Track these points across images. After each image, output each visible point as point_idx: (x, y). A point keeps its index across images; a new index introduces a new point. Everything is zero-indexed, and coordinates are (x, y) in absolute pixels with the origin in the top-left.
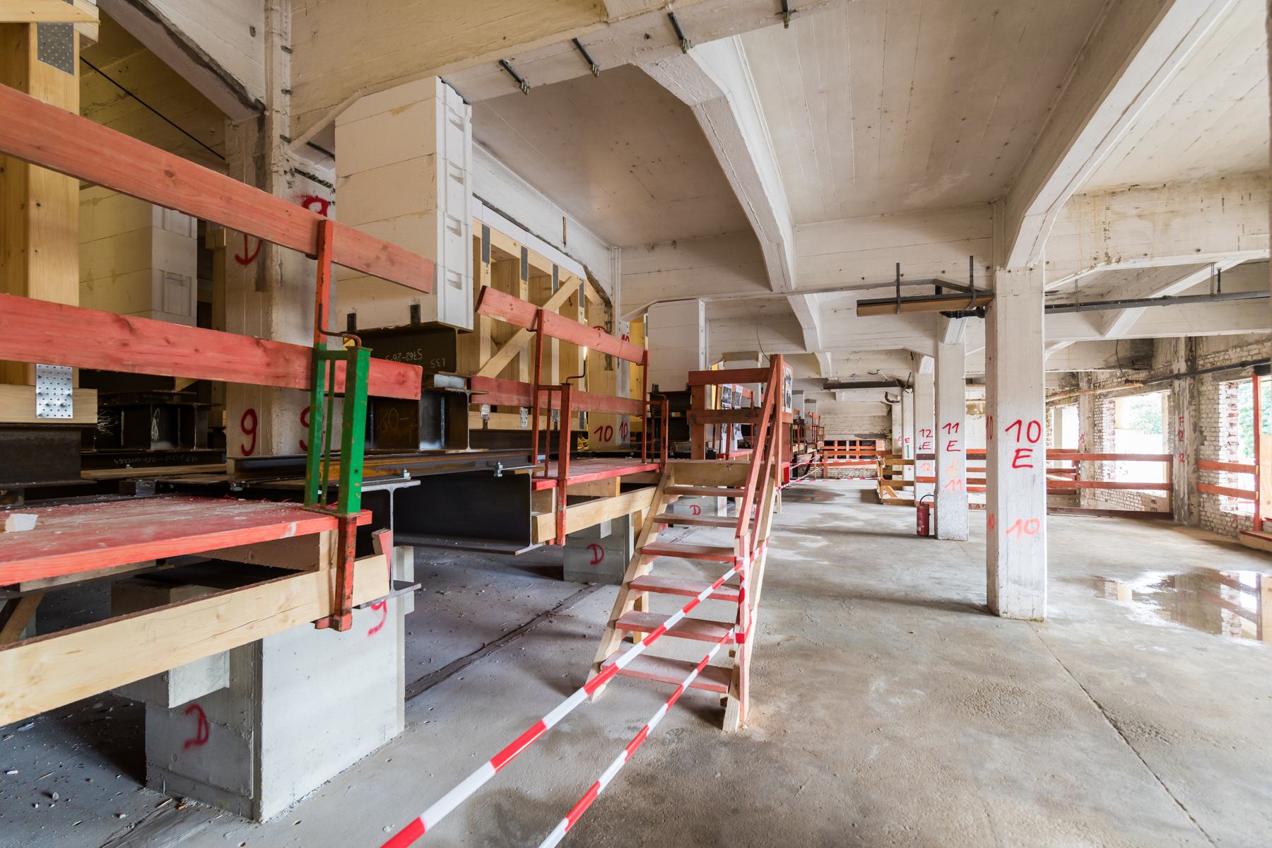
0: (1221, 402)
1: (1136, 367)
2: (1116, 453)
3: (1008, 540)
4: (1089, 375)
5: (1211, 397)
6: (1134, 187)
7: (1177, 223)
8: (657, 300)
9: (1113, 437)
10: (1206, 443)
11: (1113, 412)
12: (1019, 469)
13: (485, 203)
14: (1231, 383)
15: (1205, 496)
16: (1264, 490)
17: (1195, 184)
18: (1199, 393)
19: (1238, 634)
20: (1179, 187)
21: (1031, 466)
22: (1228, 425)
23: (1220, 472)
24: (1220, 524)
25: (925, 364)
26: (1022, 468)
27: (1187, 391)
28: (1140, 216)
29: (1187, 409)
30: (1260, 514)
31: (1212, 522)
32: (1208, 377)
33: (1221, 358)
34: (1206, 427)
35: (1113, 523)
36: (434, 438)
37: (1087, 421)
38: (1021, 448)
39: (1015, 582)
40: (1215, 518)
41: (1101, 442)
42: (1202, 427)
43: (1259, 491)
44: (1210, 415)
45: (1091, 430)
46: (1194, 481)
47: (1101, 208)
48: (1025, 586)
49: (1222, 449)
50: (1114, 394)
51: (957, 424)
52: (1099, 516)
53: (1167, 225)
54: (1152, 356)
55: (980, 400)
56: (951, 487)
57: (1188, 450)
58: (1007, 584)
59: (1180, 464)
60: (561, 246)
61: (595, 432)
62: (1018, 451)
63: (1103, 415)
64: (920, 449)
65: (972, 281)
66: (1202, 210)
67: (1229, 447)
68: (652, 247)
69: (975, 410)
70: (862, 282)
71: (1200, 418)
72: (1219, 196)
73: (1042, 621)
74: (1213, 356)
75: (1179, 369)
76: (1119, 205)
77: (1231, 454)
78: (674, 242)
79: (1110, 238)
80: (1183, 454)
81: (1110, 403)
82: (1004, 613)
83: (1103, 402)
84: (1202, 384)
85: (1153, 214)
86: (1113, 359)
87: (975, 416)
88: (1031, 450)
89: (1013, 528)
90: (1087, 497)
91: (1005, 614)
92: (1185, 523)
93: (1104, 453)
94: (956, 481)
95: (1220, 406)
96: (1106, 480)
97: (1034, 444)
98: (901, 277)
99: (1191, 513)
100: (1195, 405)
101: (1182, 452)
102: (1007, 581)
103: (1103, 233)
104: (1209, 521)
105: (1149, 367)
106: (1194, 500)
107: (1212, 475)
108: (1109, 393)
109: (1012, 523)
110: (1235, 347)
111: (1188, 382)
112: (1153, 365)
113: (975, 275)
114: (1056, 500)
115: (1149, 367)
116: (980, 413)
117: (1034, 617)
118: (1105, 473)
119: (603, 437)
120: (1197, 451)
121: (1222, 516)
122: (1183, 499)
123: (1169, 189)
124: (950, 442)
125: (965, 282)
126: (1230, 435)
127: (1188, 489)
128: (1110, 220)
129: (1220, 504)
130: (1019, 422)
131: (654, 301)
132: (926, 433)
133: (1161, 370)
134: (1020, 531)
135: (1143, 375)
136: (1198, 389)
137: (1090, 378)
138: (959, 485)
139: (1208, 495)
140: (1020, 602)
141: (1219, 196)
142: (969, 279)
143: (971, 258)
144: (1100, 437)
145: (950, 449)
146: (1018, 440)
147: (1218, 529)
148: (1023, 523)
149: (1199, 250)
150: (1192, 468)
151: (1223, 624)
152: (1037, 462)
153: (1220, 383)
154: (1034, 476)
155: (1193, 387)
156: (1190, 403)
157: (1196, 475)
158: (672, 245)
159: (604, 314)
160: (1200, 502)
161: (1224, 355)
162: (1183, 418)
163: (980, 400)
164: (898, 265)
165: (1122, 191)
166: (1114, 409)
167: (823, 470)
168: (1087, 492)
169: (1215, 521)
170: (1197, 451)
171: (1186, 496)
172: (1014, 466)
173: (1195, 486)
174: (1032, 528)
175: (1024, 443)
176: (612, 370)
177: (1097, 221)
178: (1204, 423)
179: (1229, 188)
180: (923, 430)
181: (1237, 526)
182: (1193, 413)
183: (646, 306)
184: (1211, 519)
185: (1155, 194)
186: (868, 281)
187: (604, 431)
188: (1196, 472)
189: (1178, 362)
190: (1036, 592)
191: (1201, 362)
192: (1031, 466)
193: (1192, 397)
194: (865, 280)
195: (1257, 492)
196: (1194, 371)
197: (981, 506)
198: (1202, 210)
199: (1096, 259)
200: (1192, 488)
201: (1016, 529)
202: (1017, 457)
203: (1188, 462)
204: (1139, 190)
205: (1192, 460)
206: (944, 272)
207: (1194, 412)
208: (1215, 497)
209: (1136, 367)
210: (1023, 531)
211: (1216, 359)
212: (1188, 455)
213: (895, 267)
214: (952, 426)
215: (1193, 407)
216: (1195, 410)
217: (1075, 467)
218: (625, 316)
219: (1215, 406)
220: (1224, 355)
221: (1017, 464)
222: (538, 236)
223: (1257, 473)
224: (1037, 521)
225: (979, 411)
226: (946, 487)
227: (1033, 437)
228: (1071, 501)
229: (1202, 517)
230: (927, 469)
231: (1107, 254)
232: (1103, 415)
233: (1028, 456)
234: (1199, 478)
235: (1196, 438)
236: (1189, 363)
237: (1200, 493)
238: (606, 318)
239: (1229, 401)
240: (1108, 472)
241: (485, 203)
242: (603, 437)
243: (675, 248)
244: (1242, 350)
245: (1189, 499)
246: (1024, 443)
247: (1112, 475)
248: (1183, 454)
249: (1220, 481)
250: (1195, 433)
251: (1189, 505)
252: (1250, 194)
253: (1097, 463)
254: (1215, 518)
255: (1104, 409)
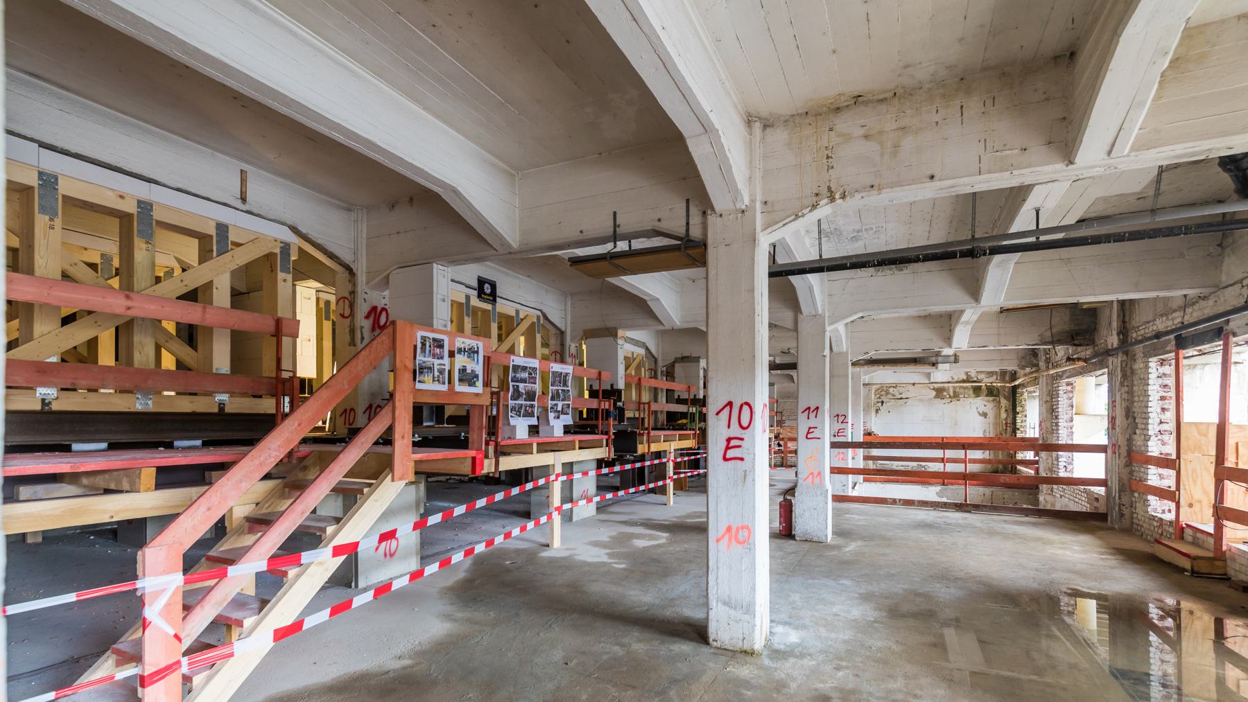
0: (1150, 382)
1: (1076, 342)
2: (1075, 443)
3: (718, 551)
4: (1047, 354)
5: (1142, 377)
6: (857, 99)
7: (908, 142)
8: (396, 266)
9: (1071, 424)
10: (1138, 431)
11: (1071, 395)
12: (729, 462)
13: (43, 145)
14: (1163, 360)
15: (1136, 495)
16: (1185, 489)
17: (930, 89)
18: (1133, 372)
19: (1169, 662)
20: (911, 95)
21: (742, 459)
22: (1159, 410)
23: (1149, 466)
24: (1148, 529)
25: (836, 341)
26: (733, 461)
27: (1119, 369)
28: (866, 137)
29: (1119, 391)
30: (1181, 520)
31: (1142, 526)
32: (1138, 349)
33: (1151, 329)
34: (1138, 412)
35: (1035, 524)
36: (431, 420)
37: (1045, 405)
38: (732, 436)
39: (726, 603)
40: (1144, 522)
41: (1058, 430)
42: (1134, 412)
43: (1179, 491)
44: (1141, 399)
45: (1049, 416)
46: (1125, 477)
47: (823, 129)
48: (735, 608)
49: (1152, 438)
50: (1067, 374)
51: (817, 408)
52: (1027, 516)
53: (896, 146)
54: (1095, 329)
55: (949, 382)
56: (810, 480)
57: (1119, 441)
58: (717, 606)
59: (1112, 456)
60: (238, 204)
61: (364, 413)
62: (729, 440)
63: (1059, 399)
64: (835, 436)
65: (687, 230)
66: (937, 123)
67: (1160, 437)
68: (393, 206)
69: (945, 393)
70: (581, 237)
71: (1133, 402)
72: (957, 103)
73: (752, 654)
74: (1144, 327)
75: (1112, 344)
76: (848, 124)
77: (1163, 445)
78: (411, 199)
79: (833, 167)
80: (1115, 445)
81: (1068, 384)
82: (714, 641)
83: (1060, 384)
84: (1135, 360)
85: (881, 133)
86: (1048, 334)
87: (944, 401)
88: (742, 439)
89: (723, 536)
90: (1045, 492)
91: (715, 643)
92: (1116, 526)
93: (1060, 442)
94: (816, 473)
95: (1150, 388)
96: (1062, 474)
97: (746, 431)
98: (617, 229)
99: (1122, 515)
100: (1127, 386)
101: (1114, 442)
102: (717, 602)
103: (825, 161)
104: (1139, 525)
105: (1092, 342)
106: (1125, 500)
107: (1142, 470)
108: (1064, 372)
109: (722, 529)
110: (1162, 315)
111: (1120, 359)
112: (1096, 339)
113: (691, 222)
114: (1014, 495)
115: (1092, 342)
116: (950, 397)
117: (745, 648)
118: (1062, 464)
119: (347, 421)
120: (1130, 441)
121: (1150, 519)
122: (1114, 498)
123: (899, 99)
124: (810, 428)
125: (681, 231)
126: (1161, 423)
127: (1119, 485)
128: (833, 143)
129: (1150, 505)
130: (730, 404)
131: (394, 268)
132: (841, 419)
133: (1103, 345)
134: (730, 540)
135: (1087, 352)
136: (1131, 367)
137: (1048, 356)
138: (818, 478)
139: (1139, 494)
140: (730, 629)
141: (957, 103)
142: (685, 228)
143: (688, 201)
144: (1057, 425)
145: (809, 436)
146: (729, 427)
147: (1147, 535)
148: (734, 531)
149: (932, 177)
150: (1124, 462)
151: (1151, 649)
152: (748, 454)
153: (1150, 360)
154: (746, 471)
155: (1126, 365)
156: (1122, 384)
157: (1128, 469)
158: (409, 202)
159: (348, 283)
160: (1132, 502)
161: (1152, 325)
162: (1115, 401)
163: (949, 382)
164: (615, 213)
165: (847, 106)
166: (1072, 392)
167: (783, 458)
168: (1044, 488)
169: (1144, 525)
170: (1130, 441)
171: (1117, 494)
172: (725, 459)
173: (1126, 482)
174: (743, 536)
175: (735, 431)
176: (355, 345)
177: (819, 145)
178: (1136, 408)
179: (969, 92)
180: (838, 415)
181: (1162, 532)
182: (1125, 396)
183: (385, 274)
184: (1141, 523)
185: (883, 107)
186: (588, 235)
187: (348, 413)
188: (1128, 466)
189: (1112, 335)
190: (746, 617)
191: (1134, 335)
192: (742, 459)
193: (1124, 376)
194: (585, 234)
195: (1177, 492)
196: (1126, 344)
197: (898, 501)
198: (937, 123)
199: (817, 195)
200: (1124, 484)
201: (726, 538)
202: (728, 448)
203: (1119, 455)
204: (866, 103)
205: (1124, 451)
206: (659, 220)
207: (1126, 395)
208: (1144, 496)
209: (1076, 342)
210: (733, 540)
211: (1147, 331)
212: (1119, 446)
213: (612, 216)
214: (811, 410)
215: (1126, 389)
216: (1128, 393)
217: (1037, 458)
218: (371, 284)
219: (1145, 388)
220: (1152, 325)
221: (728, 457)
222: (179, 190)
223: (1177, 469)
224: (747, 527)
225: (950, 396)
226: (804, 480)
227: (745, 423)
228: (1031, 497)
229: (1135, 521)
230: (842, 459)
231: (829, 188)
232: (1059, 399)
233: (739, 446)
234: (1131, 473)
235: (1129, 425)
236: (1121, 337)
237: (1133, 491)
238: (350, 288)
239: (1160, 381)
240: (1065, 464)
241: (43, 145)
242: (347, 421)
243: (412, 205)
244: (1167, 319)
245: (1120, 498)
246: (735, 431)
247: (1070, 467)
248: (1115, 445)
249: (1149, 477)
250: (1127, 420)
251: (1120, 505)
252: (994, 98)
253: (1054, 454)
254: (1144, 522)
255: (1060, 392)
